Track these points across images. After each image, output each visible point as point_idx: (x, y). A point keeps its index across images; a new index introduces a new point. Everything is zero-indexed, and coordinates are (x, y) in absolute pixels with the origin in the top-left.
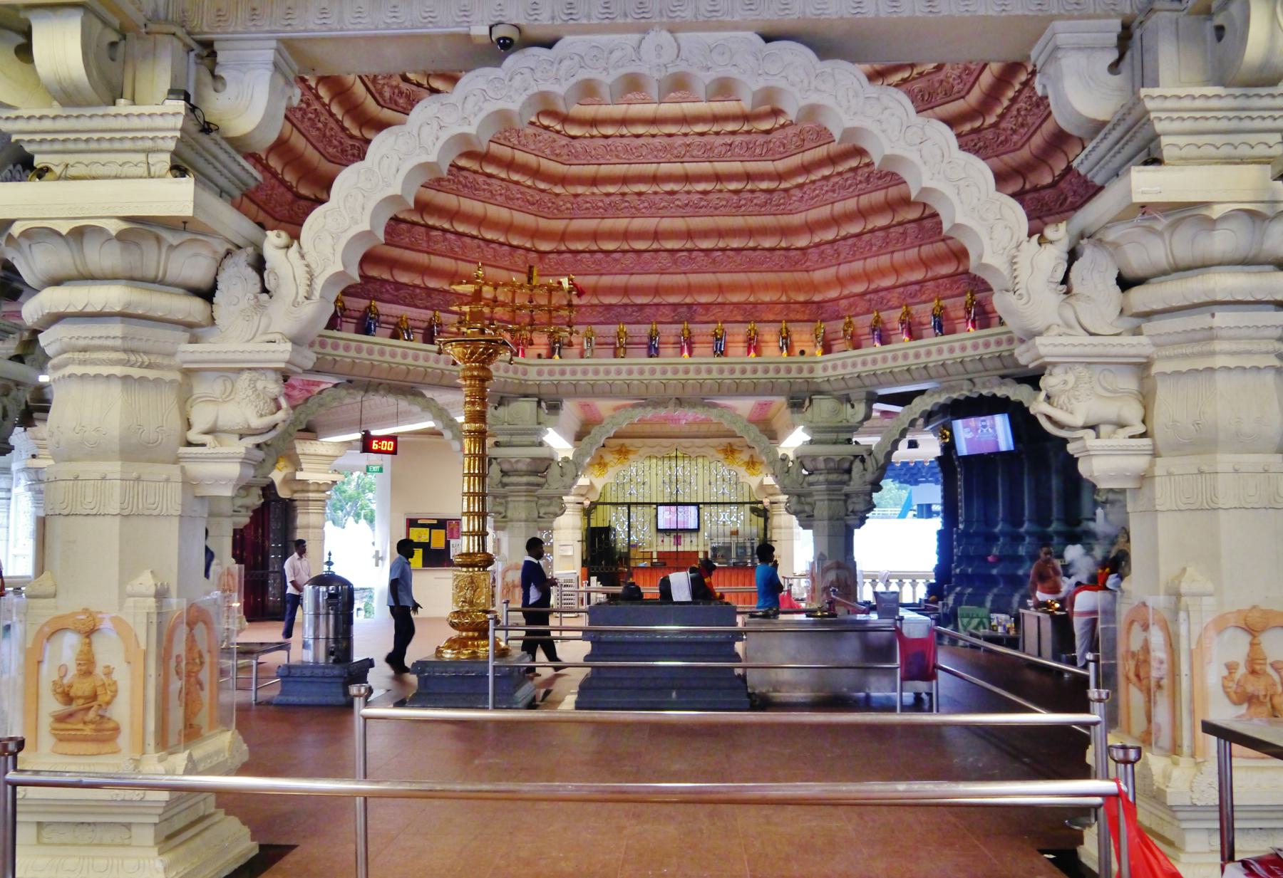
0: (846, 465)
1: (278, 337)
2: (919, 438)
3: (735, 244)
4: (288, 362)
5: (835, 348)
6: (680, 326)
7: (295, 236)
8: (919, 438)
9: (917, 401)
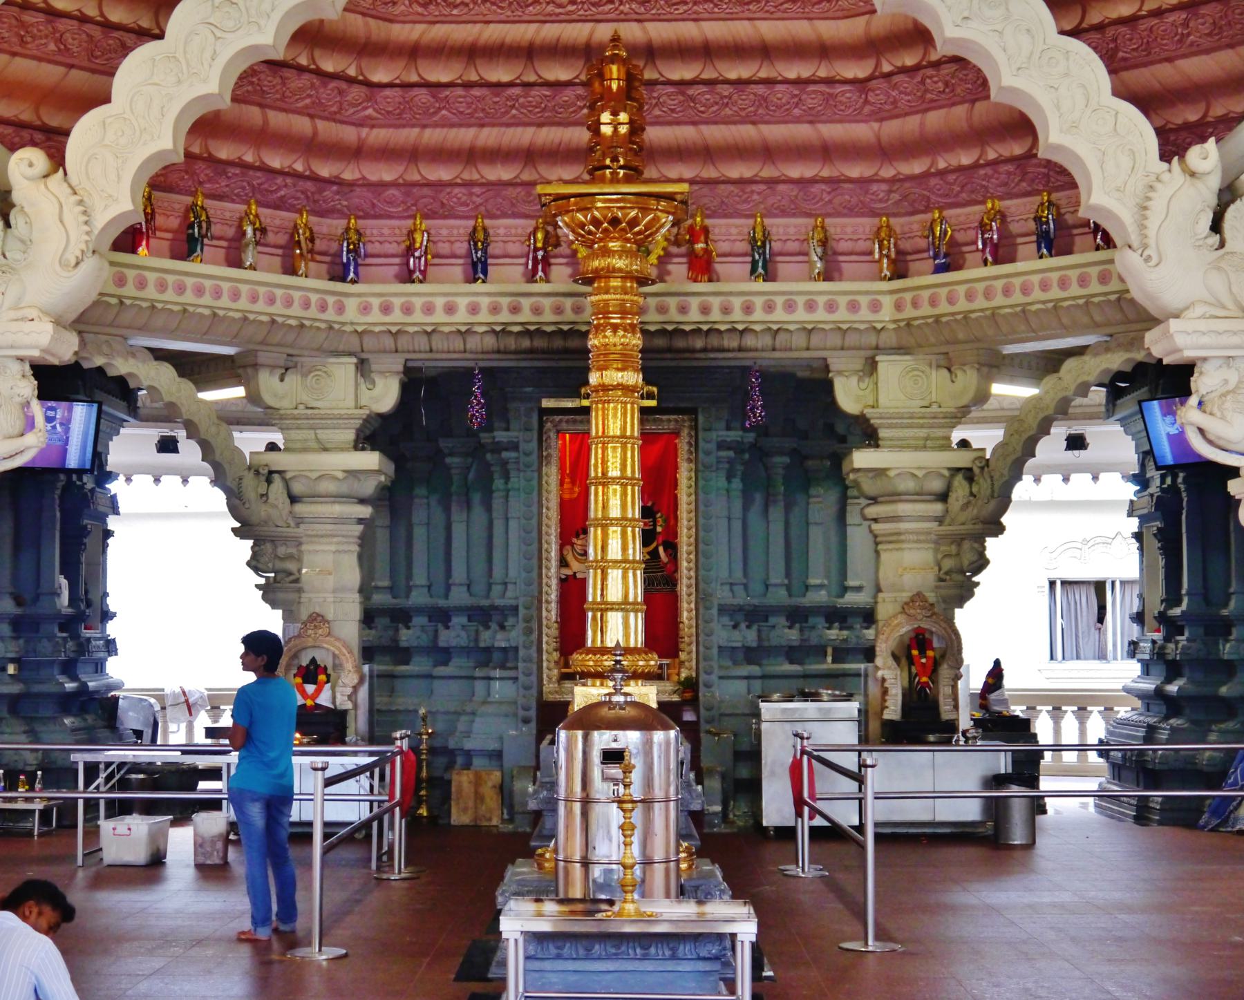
0: (937, 485)
1: (33, 313)
2: (1090, 431)
3: (734, 71)
4: (43, 351)
6: (810, 222)
7: (58, 160)
8: (1090, 431)
9: (1070, 364)
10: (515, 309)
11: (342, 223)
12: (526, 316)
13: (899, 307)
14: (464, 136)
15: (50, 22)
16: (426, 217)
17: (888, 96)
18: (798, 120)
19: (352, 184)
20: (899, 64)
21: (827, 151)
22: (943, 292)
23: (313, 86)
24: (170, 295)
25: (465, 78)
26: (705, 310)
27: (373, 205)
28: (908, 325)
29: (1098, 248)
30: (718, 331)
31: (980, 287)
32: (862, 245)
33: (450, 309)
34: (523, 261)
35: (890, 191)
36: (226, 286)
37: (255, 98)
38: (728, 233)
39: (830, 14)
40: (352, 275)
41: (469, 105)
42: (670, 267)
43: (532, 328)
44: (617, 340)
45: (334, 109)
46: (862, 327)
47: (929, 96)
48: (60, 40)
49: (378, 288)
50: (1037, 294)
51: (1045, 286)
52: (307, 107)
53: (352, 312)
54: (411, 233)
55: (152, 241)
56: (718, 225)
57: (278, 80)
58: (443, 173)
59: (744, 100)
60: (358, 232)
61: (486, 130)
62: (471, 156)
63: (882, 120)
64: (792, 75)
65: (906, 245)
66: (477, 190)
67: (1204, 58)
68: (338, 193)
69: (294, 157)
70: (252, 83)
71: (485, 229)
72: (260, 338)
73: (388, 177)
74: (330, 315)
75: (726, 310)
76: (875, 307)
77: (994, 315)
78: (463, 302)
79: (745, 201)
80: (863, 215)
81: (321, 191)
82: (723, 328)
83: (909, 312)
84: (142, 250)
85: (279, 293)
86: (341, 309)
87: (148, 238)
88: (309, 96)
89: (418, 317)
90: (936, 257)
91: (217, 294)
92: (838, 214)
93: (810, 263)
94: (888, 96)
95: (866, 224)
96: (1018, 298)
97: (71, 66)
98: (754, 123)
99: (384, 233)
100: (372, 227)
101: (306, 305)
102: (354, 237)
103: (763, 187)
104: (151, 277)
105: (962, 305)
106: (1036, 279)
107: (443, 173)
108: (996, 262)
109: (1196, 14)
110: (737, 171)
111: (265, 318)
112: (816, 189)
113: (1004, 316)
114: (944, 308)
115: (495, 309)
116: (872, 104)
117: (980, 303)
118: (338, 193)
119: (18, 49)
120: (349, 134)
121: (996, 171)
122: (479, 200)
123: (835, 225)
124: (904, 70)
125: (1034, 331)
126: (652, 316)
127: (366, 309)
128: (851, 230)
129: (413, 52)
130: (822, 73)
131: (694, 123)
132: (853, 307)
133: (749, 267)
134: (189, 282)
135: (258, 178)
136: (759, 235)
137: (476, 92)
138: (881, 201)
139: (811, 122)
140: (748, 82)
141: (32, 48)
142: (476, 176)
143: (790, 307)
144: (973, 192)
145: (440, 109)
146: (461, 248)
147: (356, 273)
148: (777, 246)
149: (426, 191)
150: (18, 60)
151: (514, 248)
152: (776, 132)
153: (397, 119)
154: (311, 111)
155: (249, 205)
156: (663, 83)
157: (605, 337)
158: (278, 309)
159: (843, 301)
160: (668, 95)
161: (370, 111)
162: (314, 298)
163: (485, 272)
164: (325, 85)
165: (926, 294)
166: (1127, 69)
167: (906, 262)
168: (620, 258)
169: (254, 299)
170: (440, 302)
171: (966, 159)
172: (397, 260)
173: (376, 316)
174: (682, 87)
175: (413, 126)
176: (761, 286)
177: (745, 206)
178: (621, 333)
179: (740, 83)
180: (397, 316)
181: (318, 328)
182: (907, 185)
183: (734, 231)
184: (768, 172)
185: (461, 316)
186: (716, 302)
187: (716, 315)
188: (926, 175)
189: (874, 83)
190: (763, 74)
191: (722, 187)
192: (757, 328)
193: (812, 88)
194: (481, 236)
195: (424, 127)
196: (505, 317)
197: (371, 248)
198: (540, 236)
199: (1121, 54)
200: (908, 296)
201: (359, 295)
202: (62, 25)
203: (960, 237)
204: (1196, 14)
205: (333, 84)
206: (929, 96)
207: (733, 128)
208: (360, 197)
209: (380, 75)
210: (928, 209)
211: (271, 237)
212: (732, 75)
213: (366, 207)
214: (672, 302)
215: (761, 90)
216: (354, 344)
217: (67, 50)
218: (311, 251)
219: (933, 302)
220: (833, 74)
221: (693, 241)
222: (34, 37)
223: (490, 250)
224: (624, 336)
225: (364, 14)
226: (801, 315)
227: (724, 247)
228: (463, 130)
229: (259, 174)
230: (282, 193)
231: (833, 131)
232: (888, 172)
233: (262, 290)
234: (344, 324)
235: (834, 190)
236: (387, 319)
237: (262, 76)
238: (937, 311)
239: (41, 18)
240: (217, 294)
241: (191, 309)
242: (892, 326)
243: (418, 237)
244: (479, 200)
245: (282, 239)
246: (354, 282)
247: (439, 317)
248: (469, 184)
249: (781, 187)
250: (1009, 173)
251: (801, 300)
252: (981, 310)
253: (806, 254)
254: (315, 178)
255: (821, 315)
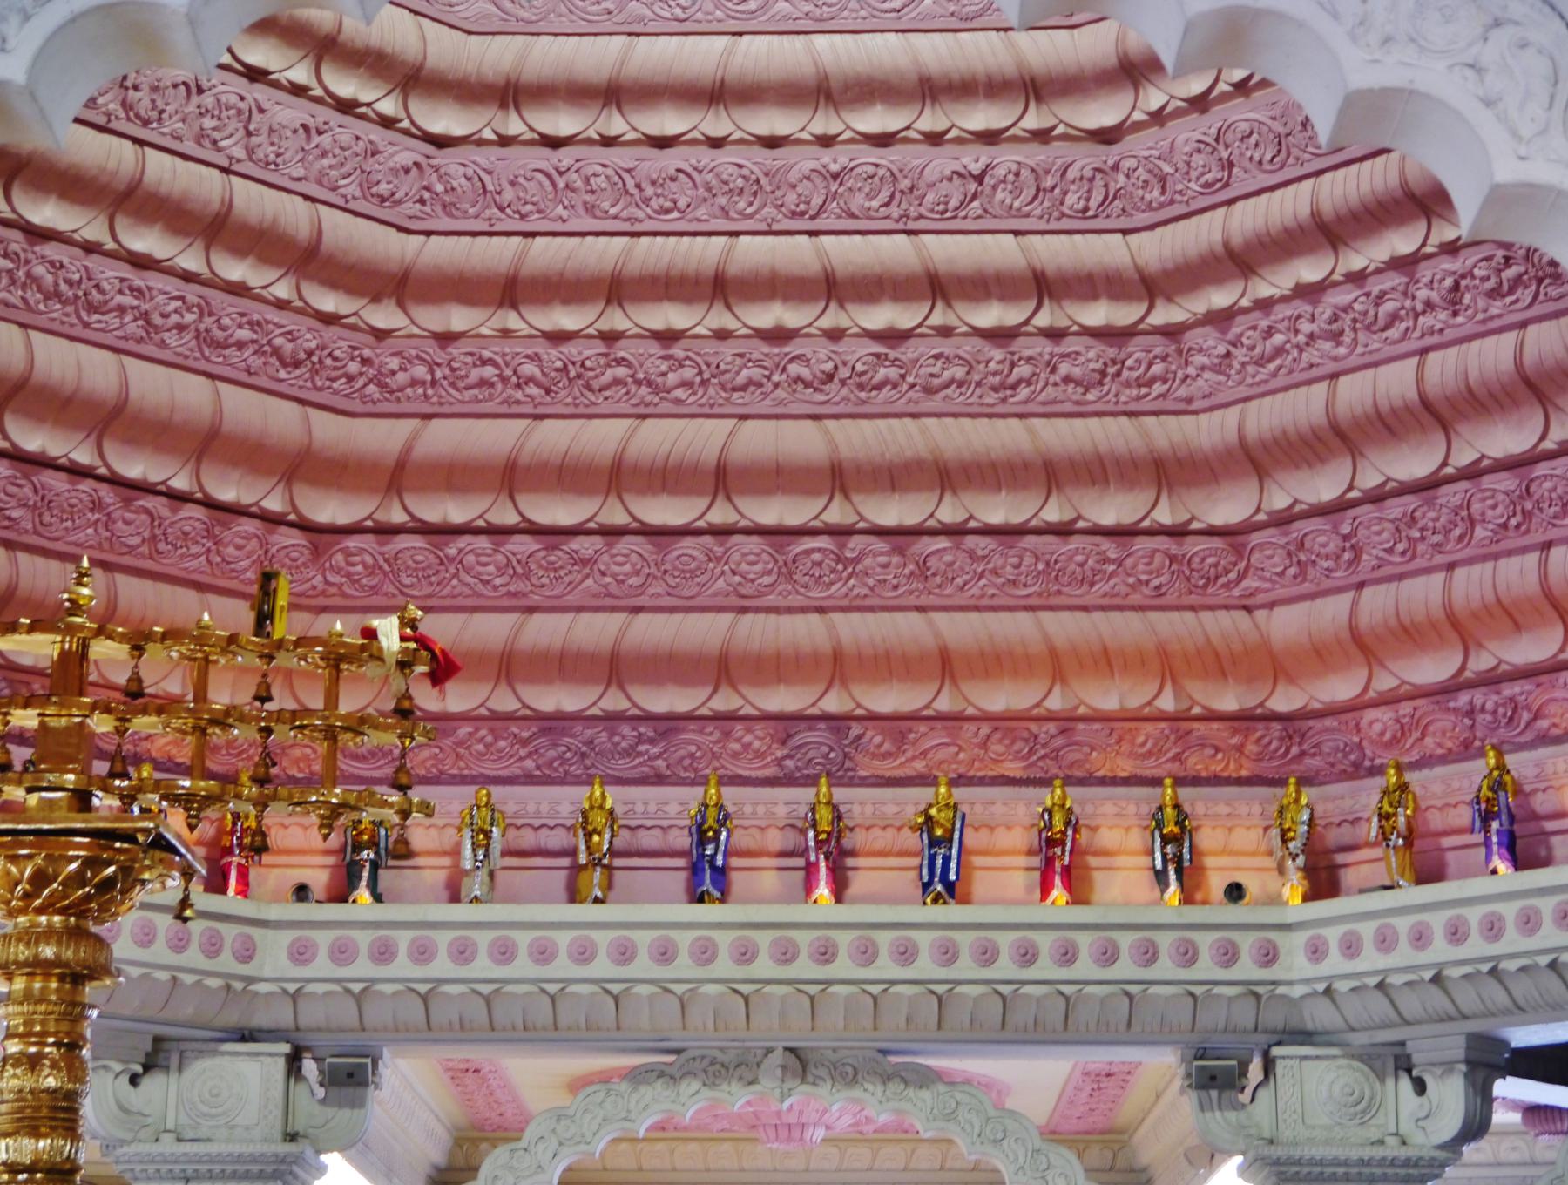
25: (601, 519)
34: (915, 861)
125: (1127, 993)
130: (1164, 515)
140: (1020, 531)
142: (623, 704)
148: (741, 839)
156: (747, 532)
167: (1088, 868)
174: (901, 540)
179: (1007, 533)
216: (282, 1016)
231: (856, 629)
234: (250, 980)
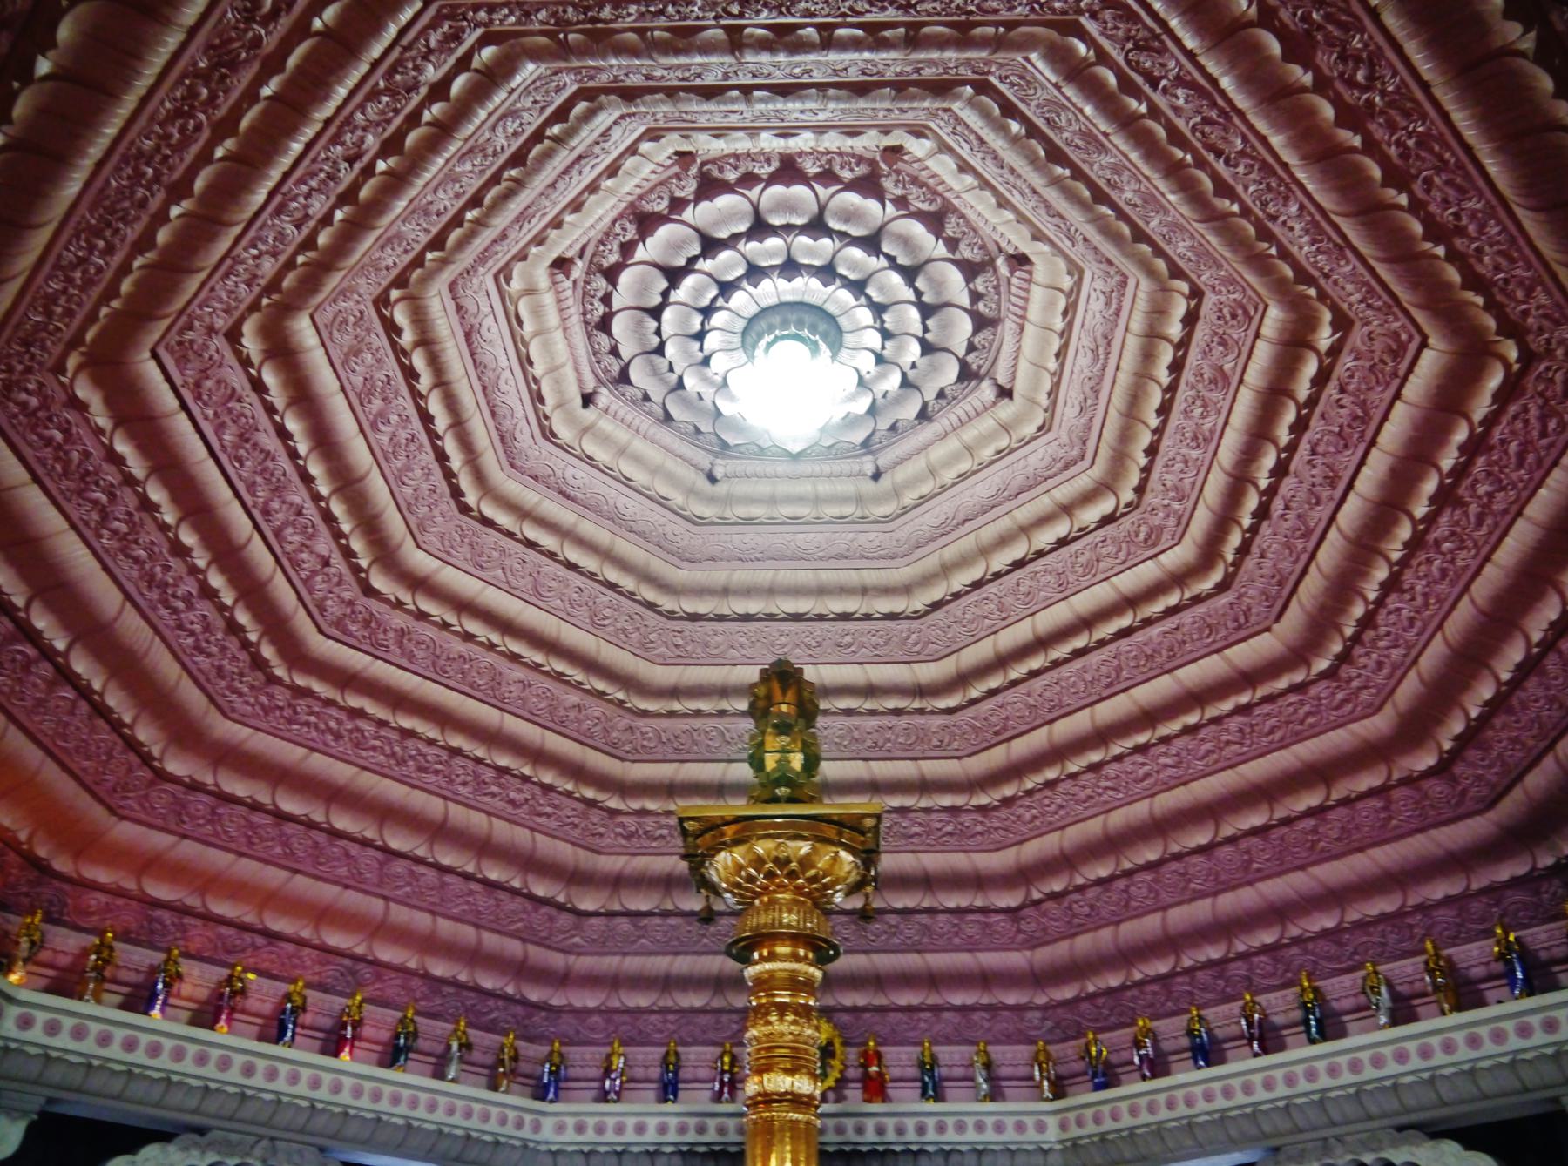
5: (949, 1093)
10: (701, 1130)
11: (546, 1049)
12: (711, 1136)
13: (1063, 1126)
14: (660, 964)
15: (277, 825)
16: (623, 1043)
17: (1038, 922)
18: (957, 949)
19: (559, 1011)
20: (1047, 890)
21: (985, 979)
22: (1106, 1109)
23: (525, 911)
24: (365, 1102)
26: (880, 1131)
27: (578, 1032)
28: (1075, 1145)
29: (1256, 1055)
30: (894, 1152)
31: (1143, 1102)
32: (1022, 1071)
33: (640, 1129)
35: (1044, 1019)
36: (424, 1097)
37: (470, 917)
38: (900, 1059)
39: (983, 847)
40: (551, 1096)
41: (665, 933)
42: (847, 1093)
43: (717, 1148)
44: (784, 1028)
45: (544, 934)
46: (1030, 1147)
47: (1077, 921)
48: (286, 844)
49: (574, 1108)
50: (1201, 1106)
51: (1209, 1097)
52: (518, 930)
53: (547, 1132)
54: (609, 1057)
55: (356, 1051)
56: (889, 1051)
57: (492, 902)
58: (642, 1000)
59: (910, 929)
60: (561, 1055)
61: (680, 959)
62: (667, 983)
63: (1033, 948)
64: (952, 904)
65: (1063, 1070)
66: (671, 1017)
67: (1335, 864)
68: (546, 1019)
69: (506, 980)
70: (468, 903)
71: (677, 1054)
72: (454, 1153)
73: (591, 1003)
74: (526, 1133)
75: (900, 1131)
76: (1041, 1127)
77: (1159, 1130)
78: (652, 1123)
79: (914, 1029)
80: (1019, 1042)
81: (529, 1016)
82: (898, 1148)
83: (1075, 1132)
84: (345, 1055)
85: (477, 1107)
86: (537, 1128)
87: (352, 1047)
88: (521, 920)
89: (609, 1137)
90: (1095, 1075)
91: (414, 1104)
92: (997, 1042)
93: (976, 1087)
94: (1038, 922)
95: (1024, 1051)
96: (1182, 1110)
97: (297, 872)
98: (919, 952)
99: (584, 1059)
100: (574, 1053)
101: (503, 1121)
102: (556, 1059)
103: (927, 1015)
104: (348, 1082)
105: (1127, 1121)
106: (1198, 1090)
107: (642, 1000)
108: (1154, 1076)
109: (1324, 820)
110: (905, 998)
111: (459, 1132)
112: (976, 1016)
113: (1169, 1130)
114: (1109, 1125)
115: (682, 1129)
116: (1023, 932)
117: (1145, 1118)
118: (546, 1019)
119: (244, 849)
120: (557, 960)
121: (1142, 993)
122: (672, 1027)
123: (998, 1052)
124: (1053, 896)
125: (1201, 1146)
126: (830, 1137)
127: (560, 1128)
128: (1010, 1056)
129: (617, 882)
130: (979, 903)
131: (866, 952)
132: (1020, 1127)
133: (919, 1091)
134: (387, 1090)
135: (471, 998)
136: (927, 1059)
137: (673, 921)
138: (1035, 1028)
139: (969, 951)
141: (259, 850)
142: (670, 1003)
143: (960, 1127)
144: (1120, 1015)
145: (640, 937)
146: (655, 1072)
147: (556, 1094)
148: (944, 1071)
149: (626, 1018)
150: (244, 861)
151: (703, 1073)
152: (939, 961)
153: (601, 947)
154: (524, 935)
155: (457, 1022)
157: (768, 1023)
158: (474, 1123)
159: (1010, 1122)
160: (843, 924)
161: (577, 940)
162: (511, 1115)
163: (676, 1096)
164: (536, 910)
165: (1089, 1113)
166: (1262, 879)
168: (790, 911)
169: (451, 1111)
170: (631, 1122)
171: (1114, 981)
172: (595, 1085)
173: (570, 1136)
175: (615, 954)
176: (931, 1106)
177: (911, 1034)
178: (790, 1018)
179: (905, 912)
180: (590, 1136)
181: (513, 1147)
182: (1060, 1011)
183: (904, 1057)
184: (933, 999)
185: (651, 1136)
186: (890, 1123)
187: (891, 1136)
188: (1077, 1000)
189: (1026, 911)
190: (926, 904)
191: (892, 1014)
192: (930, 1148)
193: (971, 917)
194: (672, 1059)
195: (625, 954)
196: (691, 1137)
197: (572, 1072)
198: (726, 1059)
199: (1255, 866)
200: (1072, 1116)
201: (555, 1114)
202: (290, 828)
203: (1114, 1059)
204: (1324, 820)
205: (545, 910)
206: (1077, 921)
207: (900, 956)
208: (567, 1024)
209: (587, 904)
210: (1081, 1034)
211: (476, 1056)
212: (899, 905)
213: (571, 1032)
214: (850, 1123)
215: (924, 919)
217: (293, 854)
218: (513, 1071)
219: (1097, 1120)
220: (987, 903)
221: (865, 1066)
222: (261, 839)
223: (683, 1074)
224: (794, 1023)
225: (573, 844)
226: (971, 1136)
227: (895, 1072)
228: (659, 959)
229: (472, 994)
230: (493, 1016)
231: (991, 959)
232: (1041, 1000)
233: (460, 1103)
234: (539, 1143)
235: (993, 1017)
236: (580, 1139)
237: (478, 897)
238: (1102, 1129)
239: (269, 820)
240: (414, 1104)
241: (385, 1118)
242: (1058, 1147)
243: (615, 1059)
244: (672, 1027)
245: (489, 1059)
246: (551, 1101)
247: (630, 1137)
248: (664, 1011)
249: (946, 1015)
250: (1155, 993)
251: (970, 1121)
252: (1147, 1125)
253: (972, 1079)
254: (524, 1002)
255: (990, 1136)
